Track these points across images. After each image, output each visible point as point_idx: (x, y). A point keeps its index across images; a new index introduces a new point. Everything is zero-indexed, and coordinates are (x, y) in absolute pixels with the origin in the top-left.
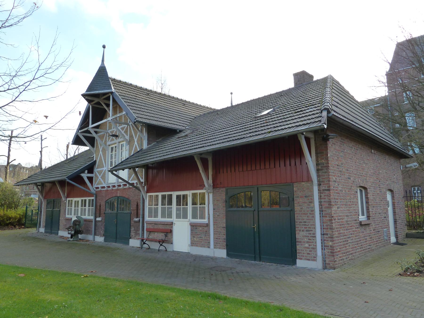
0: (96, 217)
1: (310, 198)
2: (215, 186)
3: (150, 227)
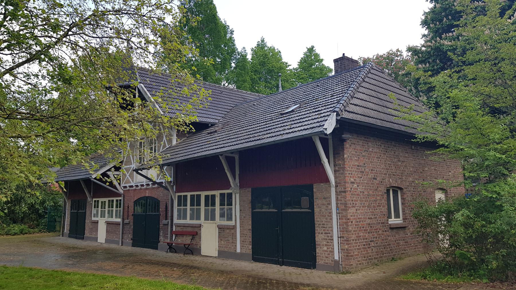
0: (123, 220)
2: (242, 186)
3: (179, 229)
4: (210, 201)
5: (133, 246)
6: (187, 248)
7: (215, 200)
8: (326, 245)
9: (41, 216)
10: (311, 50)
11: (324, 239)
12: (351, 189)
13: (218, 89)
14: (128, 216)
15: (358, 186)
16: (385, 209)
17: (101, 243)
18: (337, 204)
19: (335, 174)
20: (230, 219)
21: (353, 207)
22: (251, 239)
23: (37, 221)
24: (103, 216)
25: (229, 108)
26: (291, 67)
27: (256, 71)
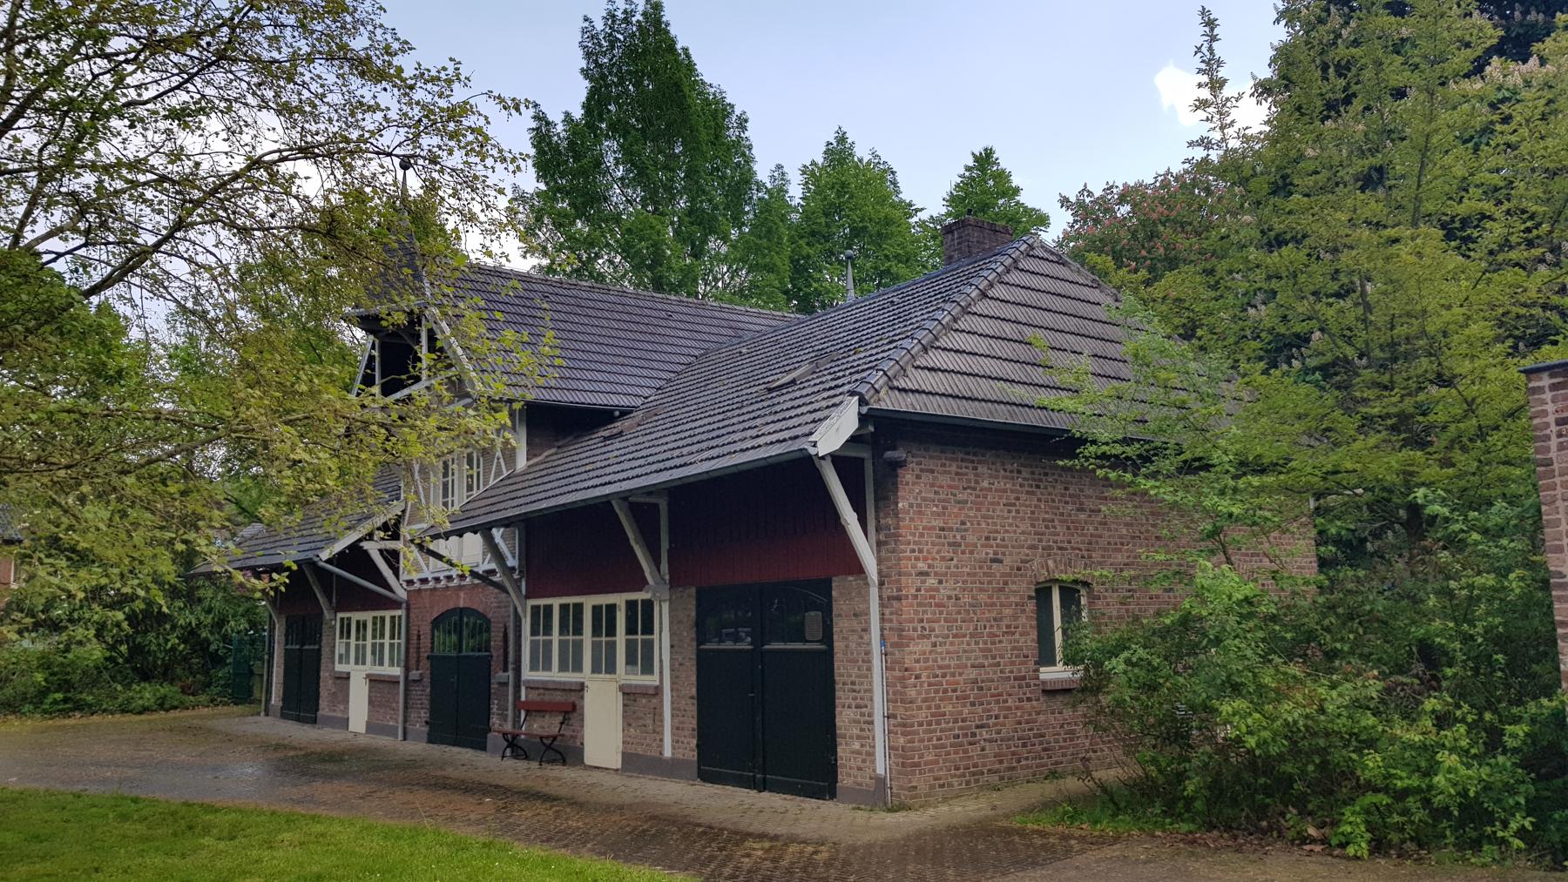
0: (407, 669)
1: (862, 615)
2: (675, 582)
3: (534, 696)
4: (605, 621)
5: (430, 741)
6: (549, 747)
7: (615, 619)
8: (859, 737)
9: (217, 660)
10: (985, 160)
11: (855, 721)
12: (918, 590)
13: (659, 306)
14: (418, 661)
15: (940, 582)
16: (1030, 641)
17: (356, 734)
18: (882, 629)
19: (879, 552)
20: (648, 669)
21: (922, 637)
22: (695, 722)
23: (207, 673)
24: (361, 660)
25: (684, 360)
26: (924, 216)
27: (813, 234)
